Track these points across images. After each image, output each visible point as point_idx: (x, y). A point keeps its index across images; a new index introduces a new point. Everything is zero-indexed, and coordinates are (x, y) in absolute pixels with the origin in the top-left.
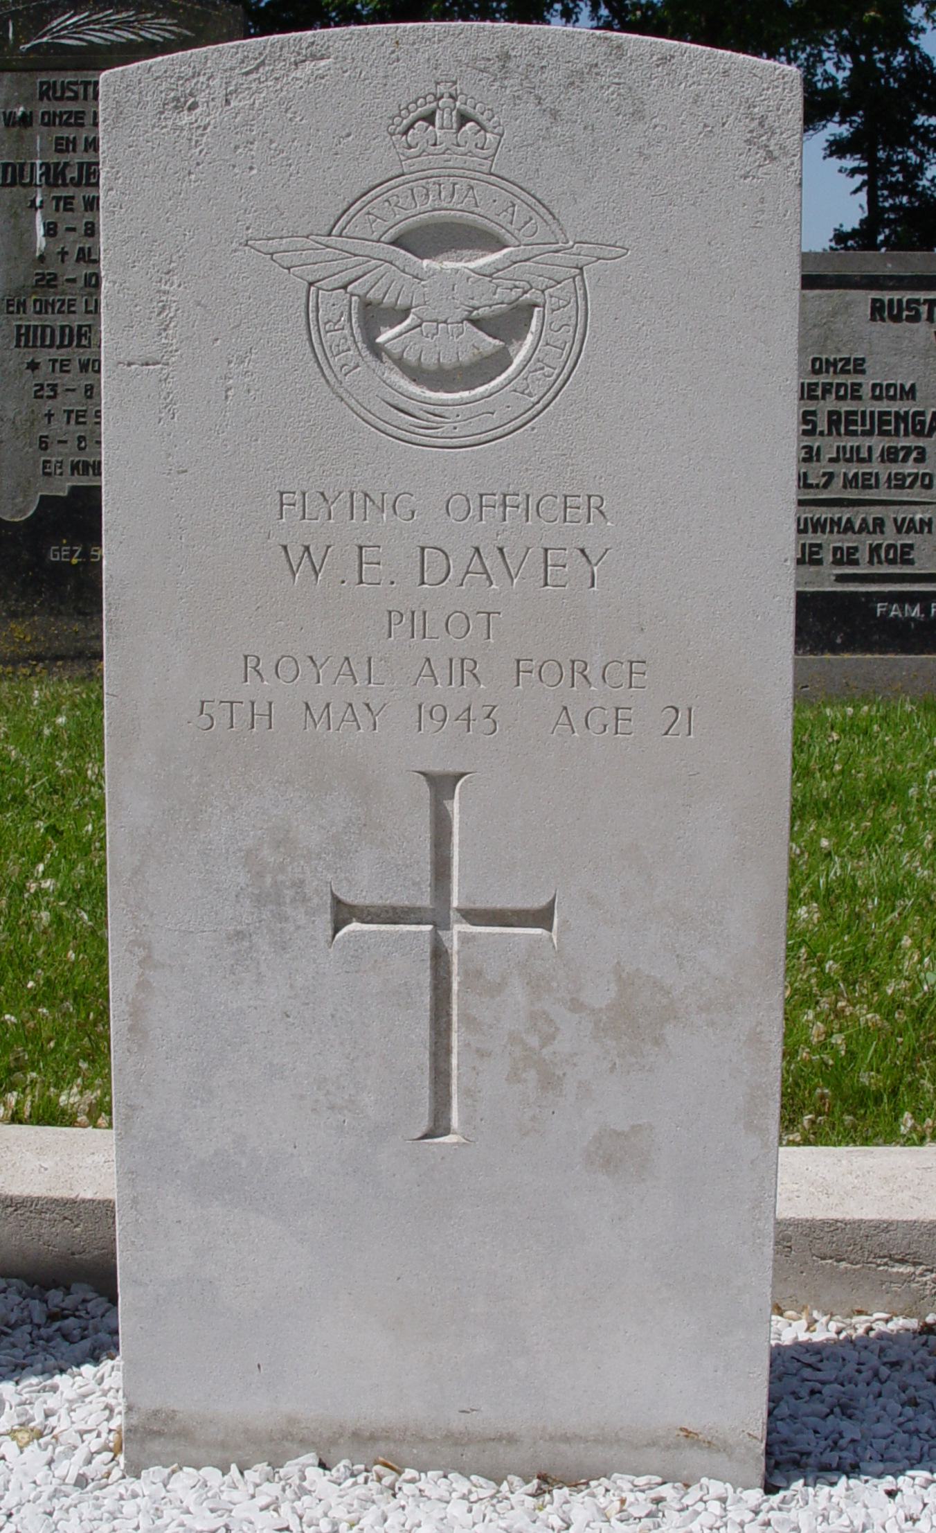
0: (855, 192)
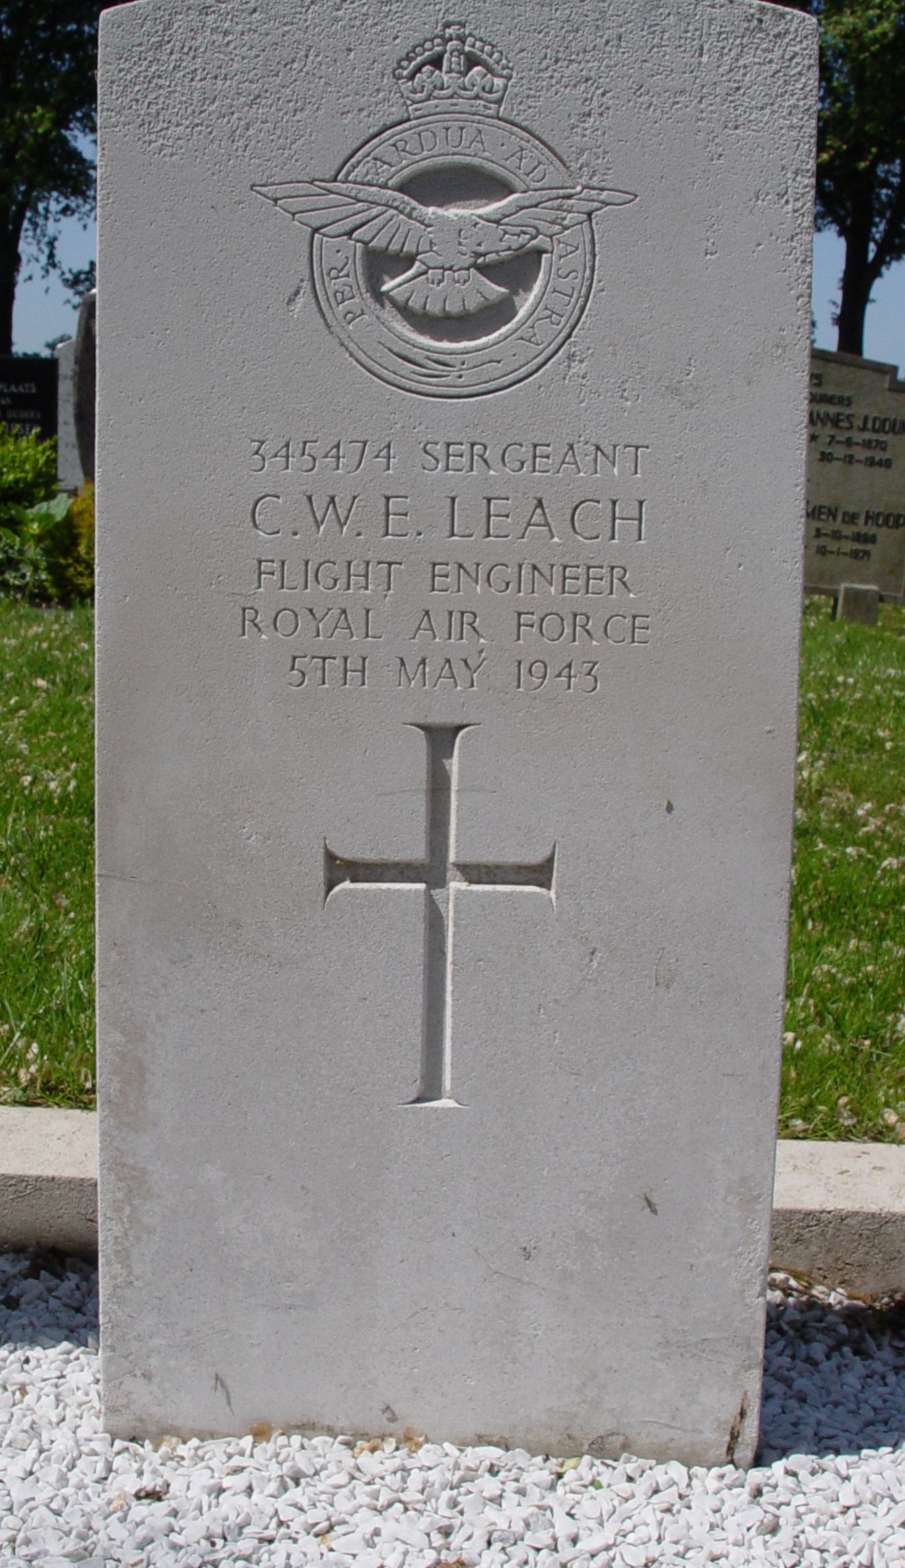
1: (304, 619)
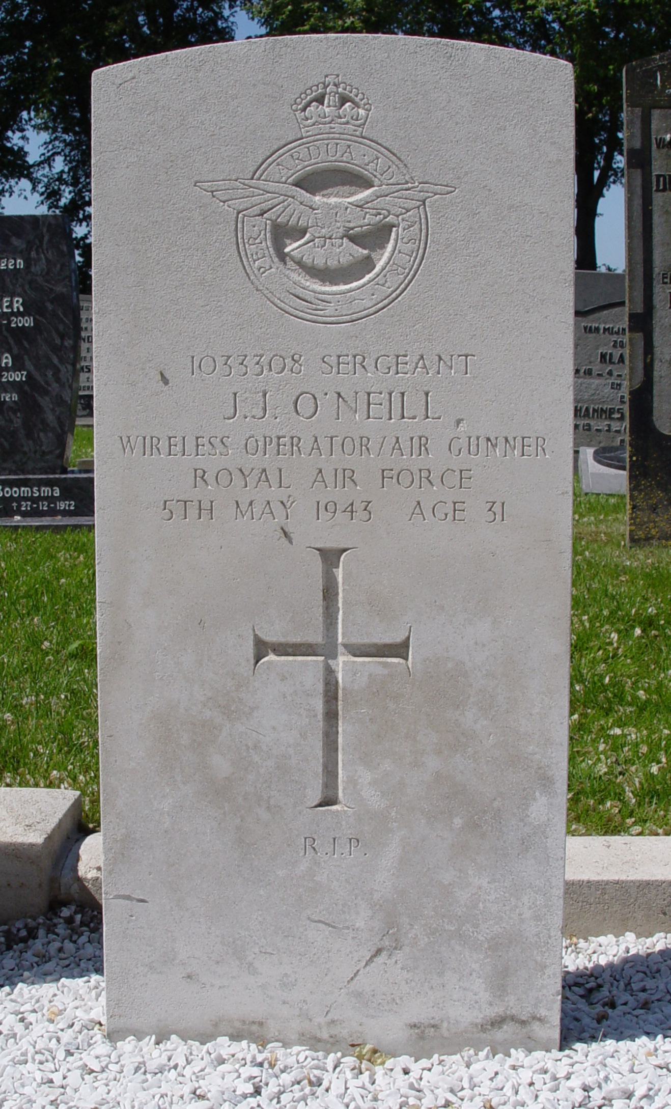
1: (236, 475)
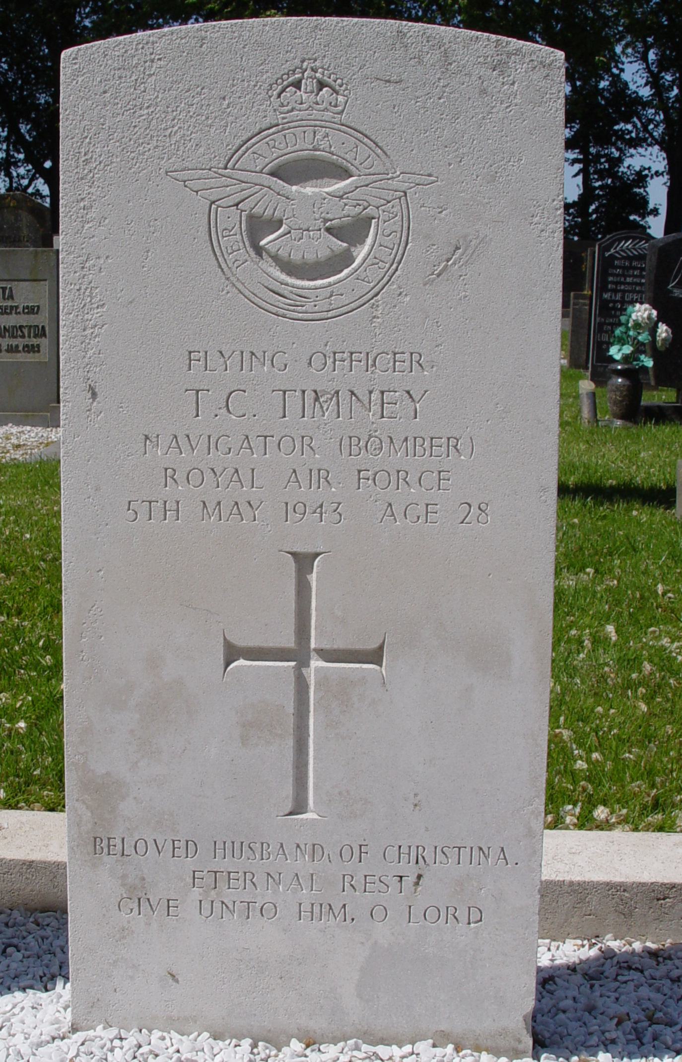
0: (575, 176)
1: (208, 475)
